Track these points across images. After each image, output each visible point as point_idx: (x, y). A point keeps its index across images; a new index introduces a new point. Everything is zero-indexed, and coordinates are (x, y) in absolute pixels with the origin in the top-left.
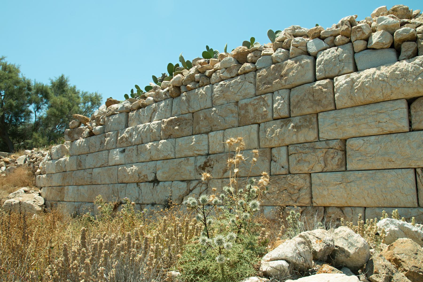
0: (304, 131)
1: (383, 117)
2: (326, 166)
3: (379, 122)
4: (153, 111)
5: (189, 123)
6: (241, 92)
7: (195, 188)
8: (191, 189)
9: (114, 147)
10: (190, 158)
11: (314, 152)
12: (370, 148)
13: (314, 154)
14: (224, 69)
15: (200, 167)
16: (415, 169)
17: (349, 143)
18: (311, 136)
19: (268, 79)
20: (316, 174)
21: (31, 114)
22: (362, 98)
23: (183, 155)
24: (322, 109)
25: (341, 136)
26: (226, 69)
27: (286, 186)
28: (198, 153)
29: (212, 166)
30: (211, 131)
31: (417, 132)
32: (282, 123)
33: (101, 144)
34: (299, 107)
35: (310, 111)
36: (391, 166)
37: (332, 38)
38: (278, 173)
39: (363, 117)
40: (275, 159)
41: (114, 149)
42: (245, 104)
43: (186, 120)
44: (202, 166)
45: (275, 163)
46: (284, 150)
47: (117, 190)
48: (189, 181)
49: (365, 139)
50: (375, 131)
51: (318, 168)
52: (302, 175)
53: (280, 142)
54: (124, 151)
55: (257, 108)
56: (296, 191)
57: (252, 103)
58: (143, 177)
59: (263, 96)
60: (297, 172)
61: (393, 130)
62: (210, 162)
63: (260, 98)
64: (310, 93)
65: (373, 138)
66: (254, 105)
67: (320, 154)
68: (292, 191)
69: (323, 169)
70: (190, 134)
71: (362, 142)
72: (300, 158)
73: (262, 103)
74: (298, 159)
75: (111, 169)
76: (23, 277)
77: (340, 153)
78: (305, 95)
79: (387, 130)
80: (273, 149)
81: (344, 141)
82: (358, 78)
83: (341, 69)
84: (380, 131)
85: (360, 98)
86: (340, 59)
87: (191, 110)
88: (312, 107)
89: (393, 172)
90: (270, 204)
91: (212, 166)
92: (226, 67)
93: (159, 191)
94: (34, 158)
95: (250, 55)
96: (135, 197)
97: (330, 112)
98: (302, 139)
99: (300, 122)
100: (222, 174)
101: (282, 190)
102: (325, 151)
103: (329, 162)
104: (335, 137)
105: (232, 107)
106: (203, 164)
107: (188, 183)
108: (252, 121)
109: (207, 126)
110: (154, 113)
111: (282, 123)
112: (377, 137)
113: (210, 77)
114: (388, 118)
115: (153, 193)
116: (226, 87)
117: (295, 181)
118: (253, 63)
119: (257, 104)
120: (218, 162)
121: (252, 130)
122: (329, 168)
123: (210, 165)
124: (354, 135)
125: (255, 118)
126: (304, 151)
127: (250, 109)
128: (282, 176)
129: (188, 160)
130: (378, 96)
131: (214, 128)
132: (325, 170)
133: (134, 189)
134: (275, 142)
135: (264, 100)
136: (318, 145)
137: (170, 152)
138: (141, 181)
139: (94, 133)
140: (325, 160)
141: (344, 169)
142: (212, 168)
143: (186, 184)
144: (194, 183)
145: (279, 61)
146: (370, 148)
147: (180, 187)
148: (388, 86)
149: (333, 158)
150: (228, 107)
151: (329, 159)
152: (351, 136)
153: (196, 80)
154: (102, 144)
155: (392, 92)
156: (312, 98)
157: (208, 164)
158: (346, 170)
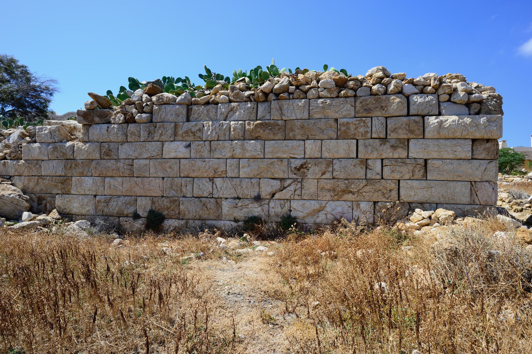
0: (400, 150)
1: (459, 149)
2: (413, 176)
3: (455, 151)
4: (230, 110)
5: (282, 129)
6: (342, 112)
7: (289, 185)
8: (285, 186)
9: (172, 139)
10: (284, 160)
11: (406, 165)
12: (446, 167)
13: (406, 167)
14: (323, 89)
15: (295, 168)
16: (471, 182)
17: (429, 162)
18: (404, 154)
19: (369, 106)
20: (405, 181)
21: (237, 73)
22: (447, 134)
23: (275, 156)
24: (415, 137)
25: (425, 158)
26: (325, 89)
27: (380, 188)
28: (292, 156)
29: (308, 168)
30: (308, 139)
31: (475, 160)
32: (381, 142)
33: (149, 134)
34: (396, 132)
35: (405, 137)
36: (459, 179)
37: (422, 87)
38: (373, 178)
39: (445, 147)
40: (371, 168)
41: (172, 141)
42: (347, 122)
43: (279, 125)
44: (298, 167)
45: (370, 171)
46: (379, 163)
47: (180, 184)
48: (282, 180)
49: (443, 161)
50: (451, 156)
51: (407, 176)
52: (394, 181)
53: (378, 156)
54: (189, 146)
55: (357, 128)
56: (389, 192)
57: (354, 123)
58: (220, 173)
59: (364, 119)
60: (390, 178)
61: (463, 157)
62: (306, 165)
63: (360, 120)
64: (406, 124)
65: (448, 161)
66: (355, 125)
67: (410, 167)
68: (385, 191)
69: (410, 178)
70: (216, 139)
71: (441, 162)
72: (394, 169)
73: (362, 124)
74: (392, 169)
75: (168, 162)
76: (51, 276)
77: (424, 168)
78: (402, 125)
79: (458, 157)
80: (368, 160)
81: (426, 161)
82: (446, 121)
83: (430, 111)
84: (454, 157)
85: (444, 134)
86: (430, 104)
87: (284, 118)
88: (407, 134)
89: (460, 183)
90: (365, 200)
91: (308, 168)
92: (325, 87)
93: (244, 187)
94: (75, 135)
95: (351, 83)
96: (208, 191)
97: (419, 140)
98: (396, 156)
99: (396, 143)
100: (320, 175)
101: (377, 190)
102: (414, 165)
103: (416, 173)
104: (421, 157)
105: (332, 122)
106: (299, 165)
107: (281, 181)
108: (352, 137)
109: (304, 134)
110: (231, 113)
111: (381, 142)
112: (451, 161)
113: (306, 92)
114: (461, 149)
115: (237, 188)
116: (328, 105)
117: (388, 185)
118: (355, 91)
119: (358, 124)
120: (318, 166)
121: (352, 143)
122: (415, 177)
123: (306, 167)
124: (436, 157)
125: (355, 135)
126: (399, 164)
127: (352, 127)
128: (377, 180)
129: (282, 161)
130: (458, 135)
131: (310, 137)
132: (412, 178)
133: (207, 184)
134: (374, 155)
135: (364, 122)
136: (408, 161)
137: (260, 153)
138: (217, 176)
139: (136, 120)
140: (413, 172)
141: (425, 179)
142: (308, 169)
143: (279, 182)
144: (288, 182)
145: (380, 94)
146: (446, 167)
147: (272, 184)
148: (467, 130)
149: (419, 171)
150: (328, 121)
151: (417, 171)
152: (434, 158)
153: (290, 91)
154: (151, 134)
155: (468, 134)
156: (408, 128)
157: (304, 166)
158: (426, 179)
